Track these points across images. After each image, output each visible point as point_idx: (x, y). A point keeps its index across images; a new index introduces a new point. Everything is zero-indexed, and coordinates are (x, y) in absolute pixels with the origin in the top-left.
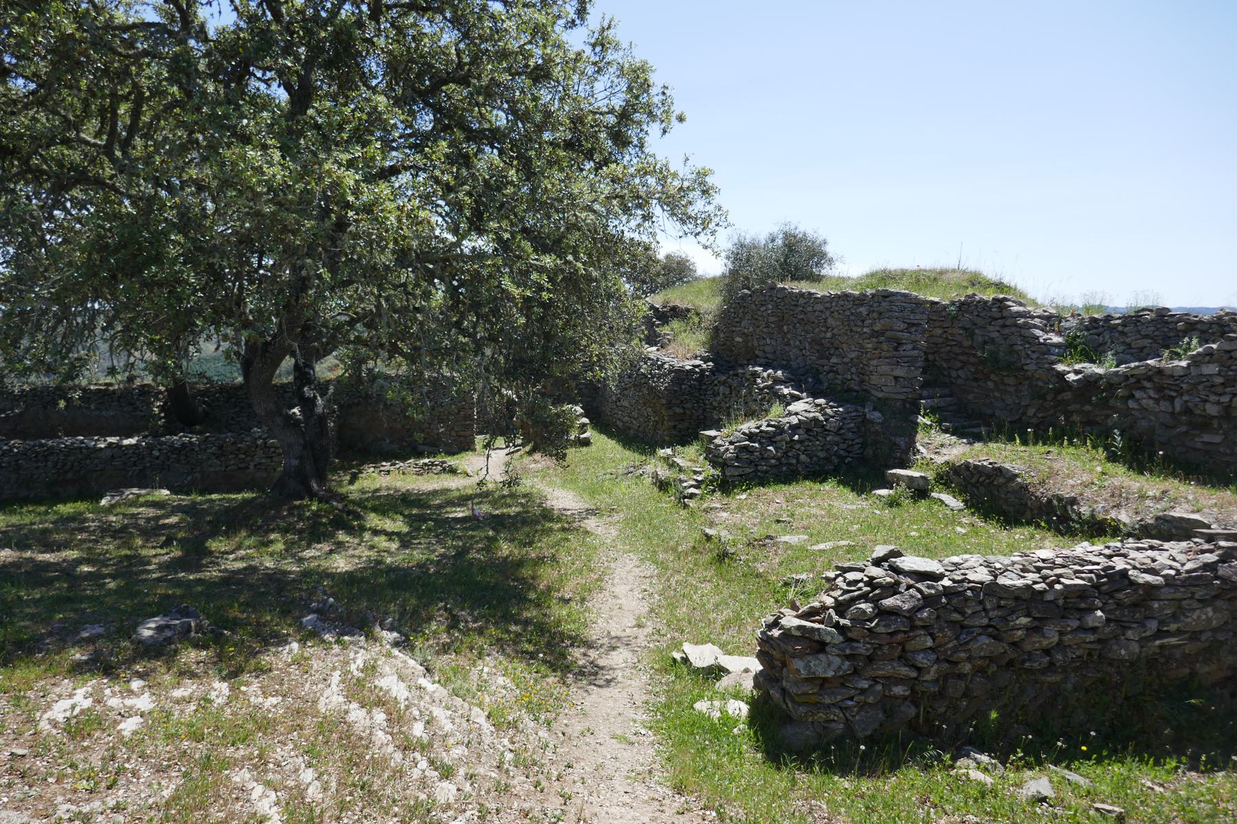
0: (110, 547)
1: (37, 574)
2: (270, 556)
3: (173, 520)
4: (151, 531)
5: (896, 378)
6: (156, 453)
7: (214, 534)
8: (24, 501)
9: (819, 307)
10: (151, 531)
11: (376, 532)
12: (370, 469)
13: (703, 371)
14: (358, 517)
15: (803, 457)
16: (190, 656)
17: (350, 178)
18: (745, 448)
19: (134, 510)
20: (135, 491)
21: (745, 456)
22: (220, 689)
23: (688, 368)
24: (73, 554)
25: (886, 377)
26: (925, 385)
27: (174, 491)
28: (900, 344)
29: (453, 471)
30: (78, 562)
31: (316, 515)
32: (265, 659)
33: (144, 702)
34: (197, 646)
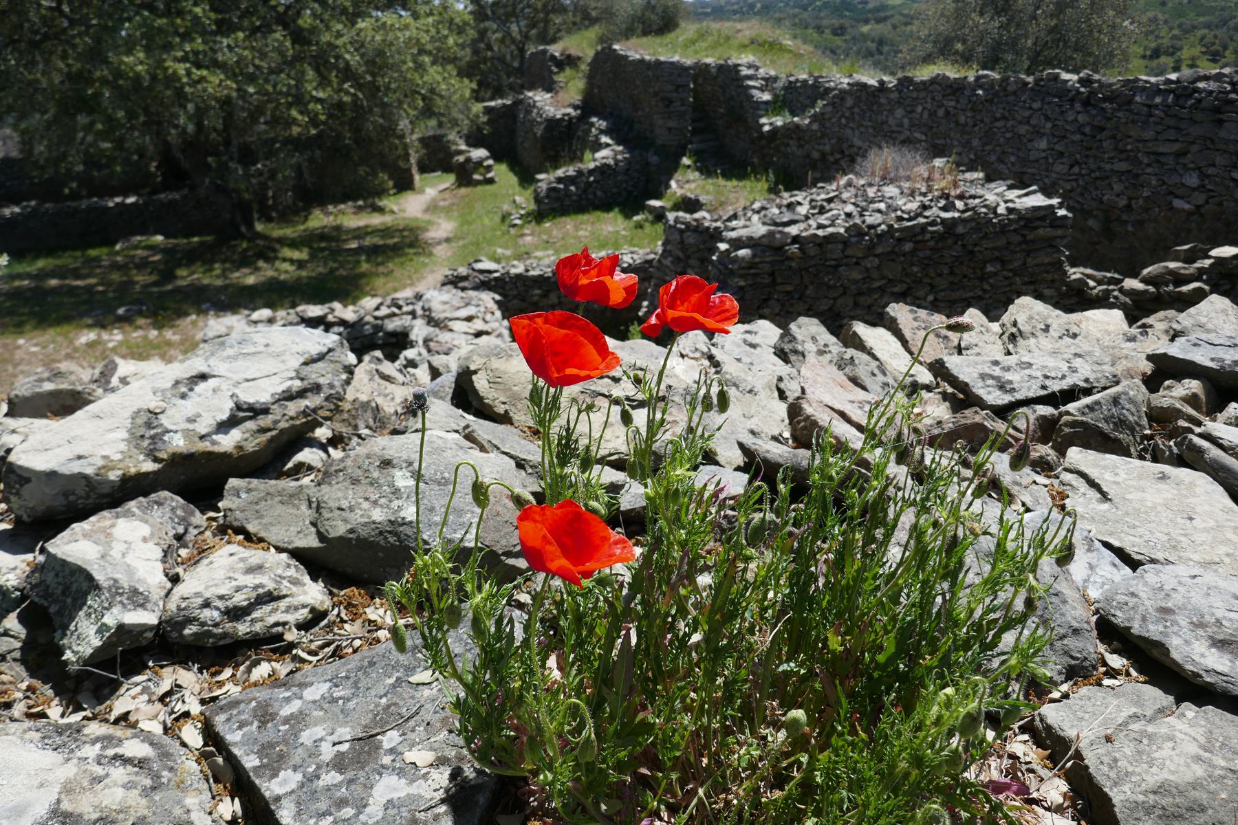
0: (115, 277)
1: (72, 291)
2: (211, 278)
3: (156, 258)
4: (143, 265)
5: (670, 129)
6: (151, 208)
7: (179, 266)
8: (65, 249)
9: (631, 68)
10: (143, 265)
11: (284, 260)
12: (317, 212)
13: (571, 119)
14: (275, 250)
15: (599, 193)
16: (141, 321)
17: (181, 69)
18: (554, 189)
19: (132, 253)
20: (139, 238)
21: (553, 194)
22: (153, 333)
23: (558, 117)
24: (92, 281)
25: (662, 128)
26: (694, 132)
27: (167, 236)
28: (671, 102)
29: (381, 210)
30: (95, 285)
31: (245, 250)
32: (178, 322)
33: (119, 337)
34: (146, 317)
